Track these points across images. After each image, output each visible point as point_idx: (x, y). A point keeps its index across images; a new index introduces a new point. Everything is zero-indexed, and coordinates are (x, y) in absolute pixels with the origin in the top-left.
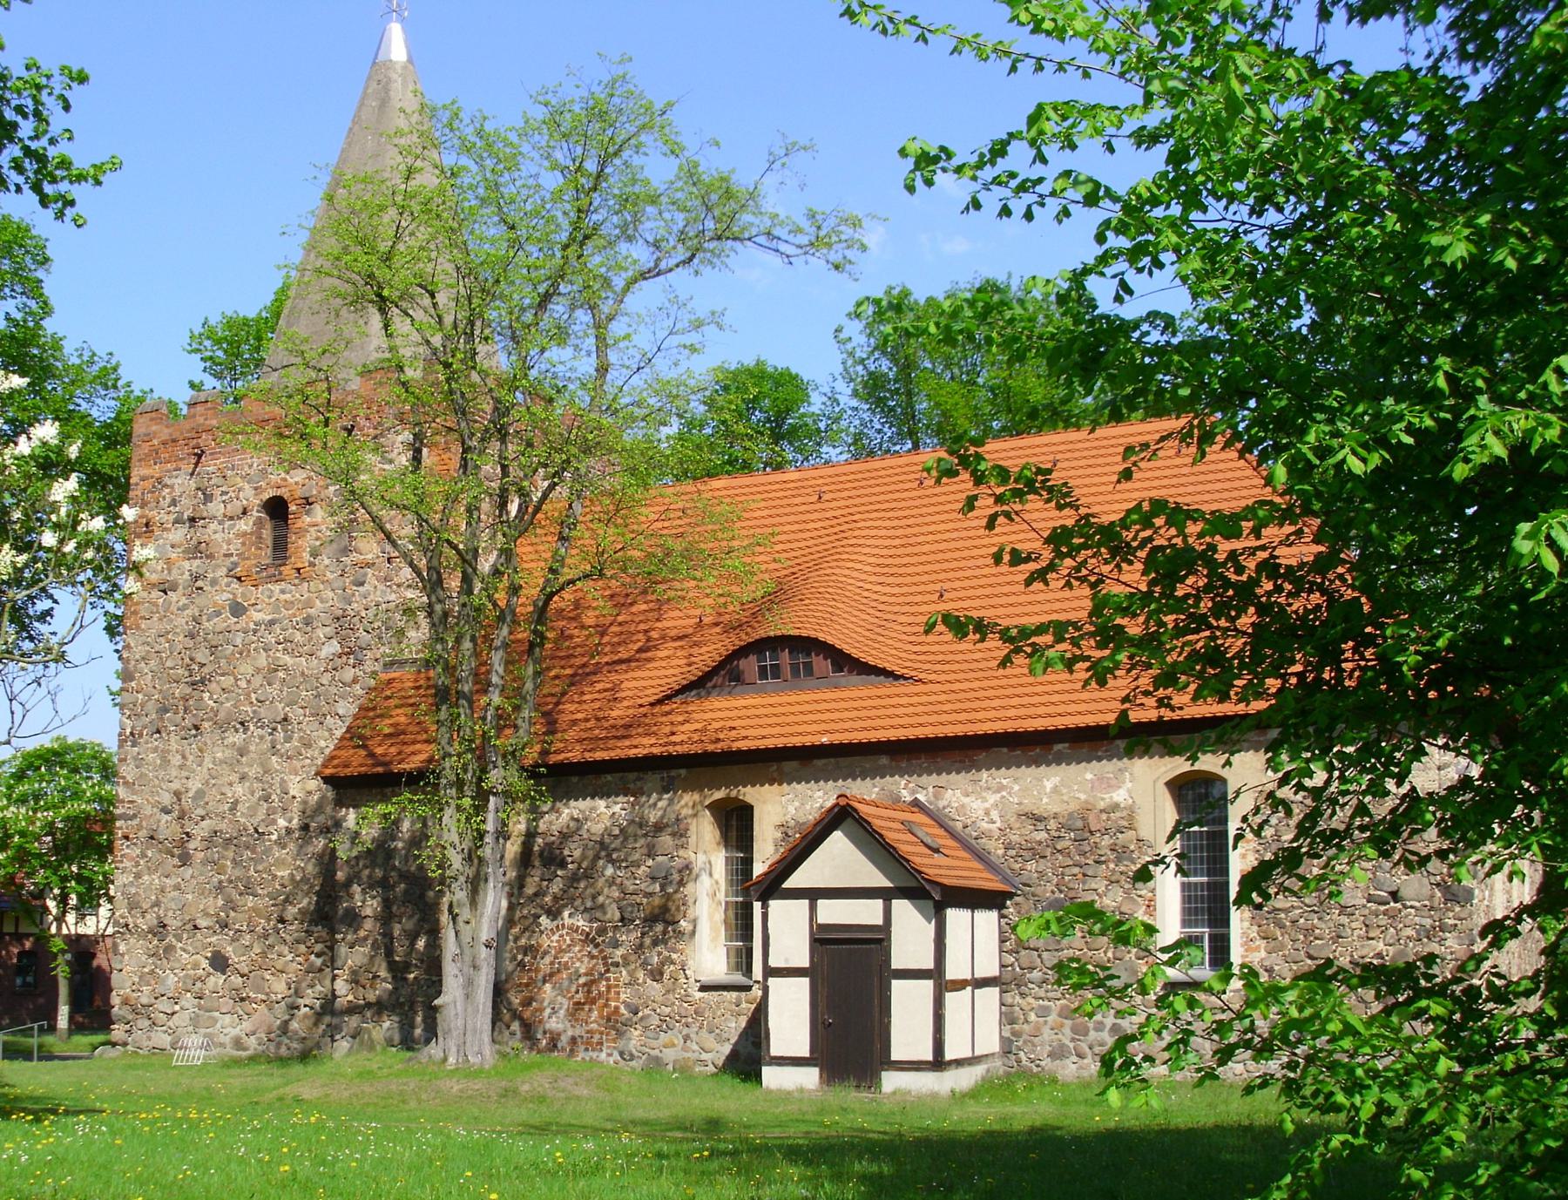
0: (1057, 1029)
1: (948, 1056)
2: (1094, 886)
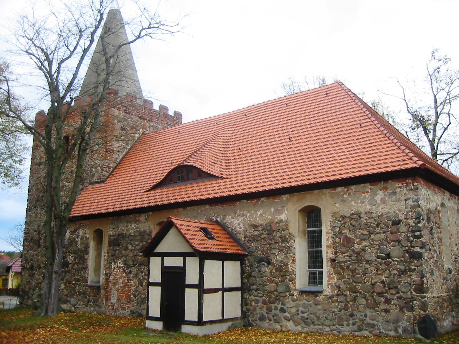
0: (261, 308)
1: (205, 319)
2: (274, 252)
